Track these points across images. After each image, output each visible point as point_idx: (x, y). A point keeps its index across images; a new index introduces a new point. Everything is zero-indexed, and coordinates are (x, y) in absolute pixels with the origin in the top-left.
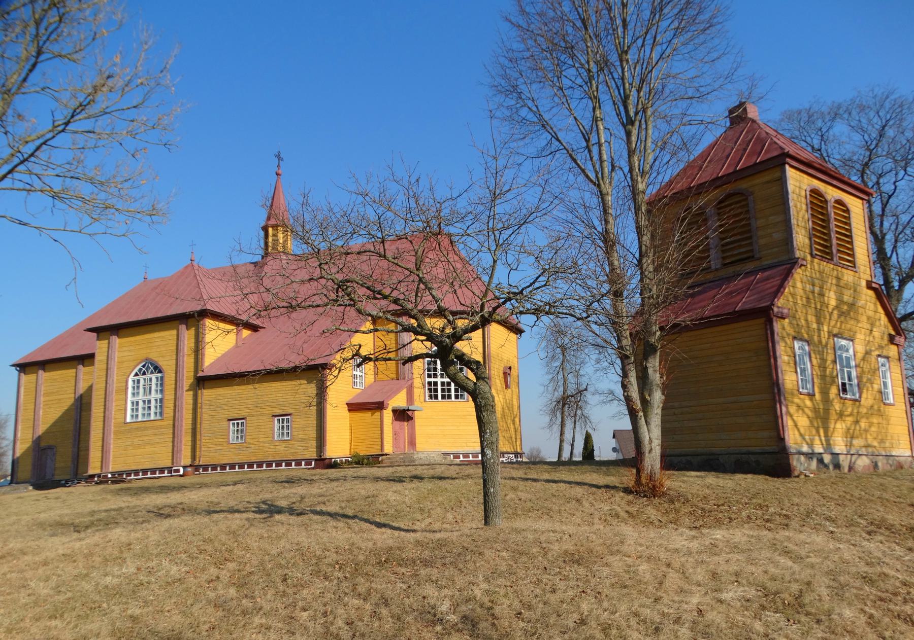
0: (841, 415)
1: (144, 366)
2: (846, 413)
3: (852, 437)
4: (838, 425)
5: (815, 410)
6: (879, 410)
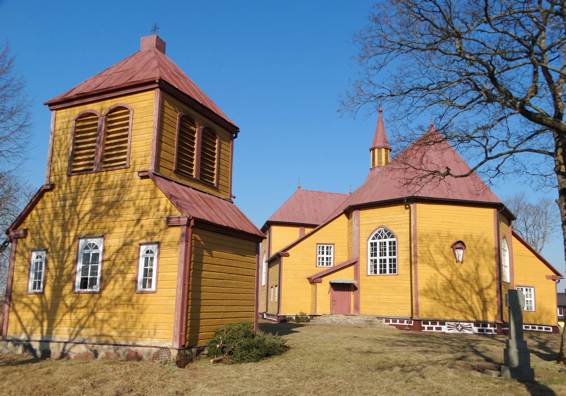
0: (72, 308)
1: (379, 232)
2: (79, 306)
3: (82, 327)
4: (67, 317)
5: (43, 306)
6: (130, 300)
